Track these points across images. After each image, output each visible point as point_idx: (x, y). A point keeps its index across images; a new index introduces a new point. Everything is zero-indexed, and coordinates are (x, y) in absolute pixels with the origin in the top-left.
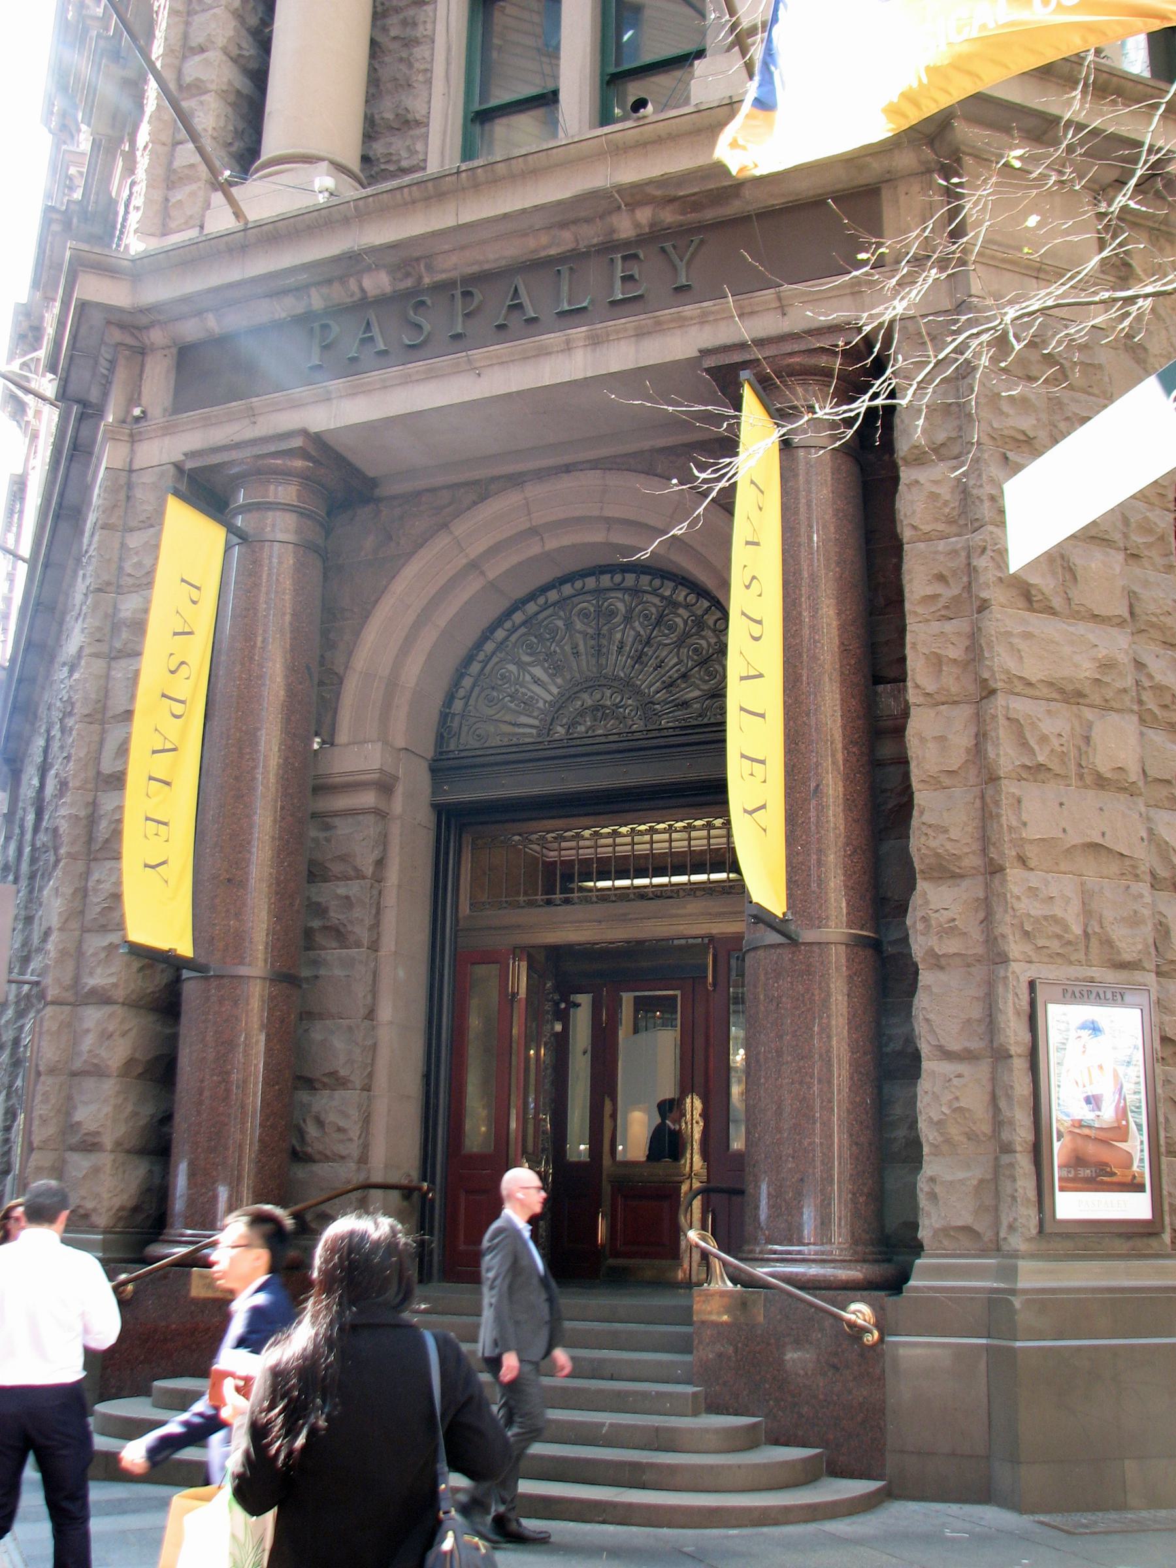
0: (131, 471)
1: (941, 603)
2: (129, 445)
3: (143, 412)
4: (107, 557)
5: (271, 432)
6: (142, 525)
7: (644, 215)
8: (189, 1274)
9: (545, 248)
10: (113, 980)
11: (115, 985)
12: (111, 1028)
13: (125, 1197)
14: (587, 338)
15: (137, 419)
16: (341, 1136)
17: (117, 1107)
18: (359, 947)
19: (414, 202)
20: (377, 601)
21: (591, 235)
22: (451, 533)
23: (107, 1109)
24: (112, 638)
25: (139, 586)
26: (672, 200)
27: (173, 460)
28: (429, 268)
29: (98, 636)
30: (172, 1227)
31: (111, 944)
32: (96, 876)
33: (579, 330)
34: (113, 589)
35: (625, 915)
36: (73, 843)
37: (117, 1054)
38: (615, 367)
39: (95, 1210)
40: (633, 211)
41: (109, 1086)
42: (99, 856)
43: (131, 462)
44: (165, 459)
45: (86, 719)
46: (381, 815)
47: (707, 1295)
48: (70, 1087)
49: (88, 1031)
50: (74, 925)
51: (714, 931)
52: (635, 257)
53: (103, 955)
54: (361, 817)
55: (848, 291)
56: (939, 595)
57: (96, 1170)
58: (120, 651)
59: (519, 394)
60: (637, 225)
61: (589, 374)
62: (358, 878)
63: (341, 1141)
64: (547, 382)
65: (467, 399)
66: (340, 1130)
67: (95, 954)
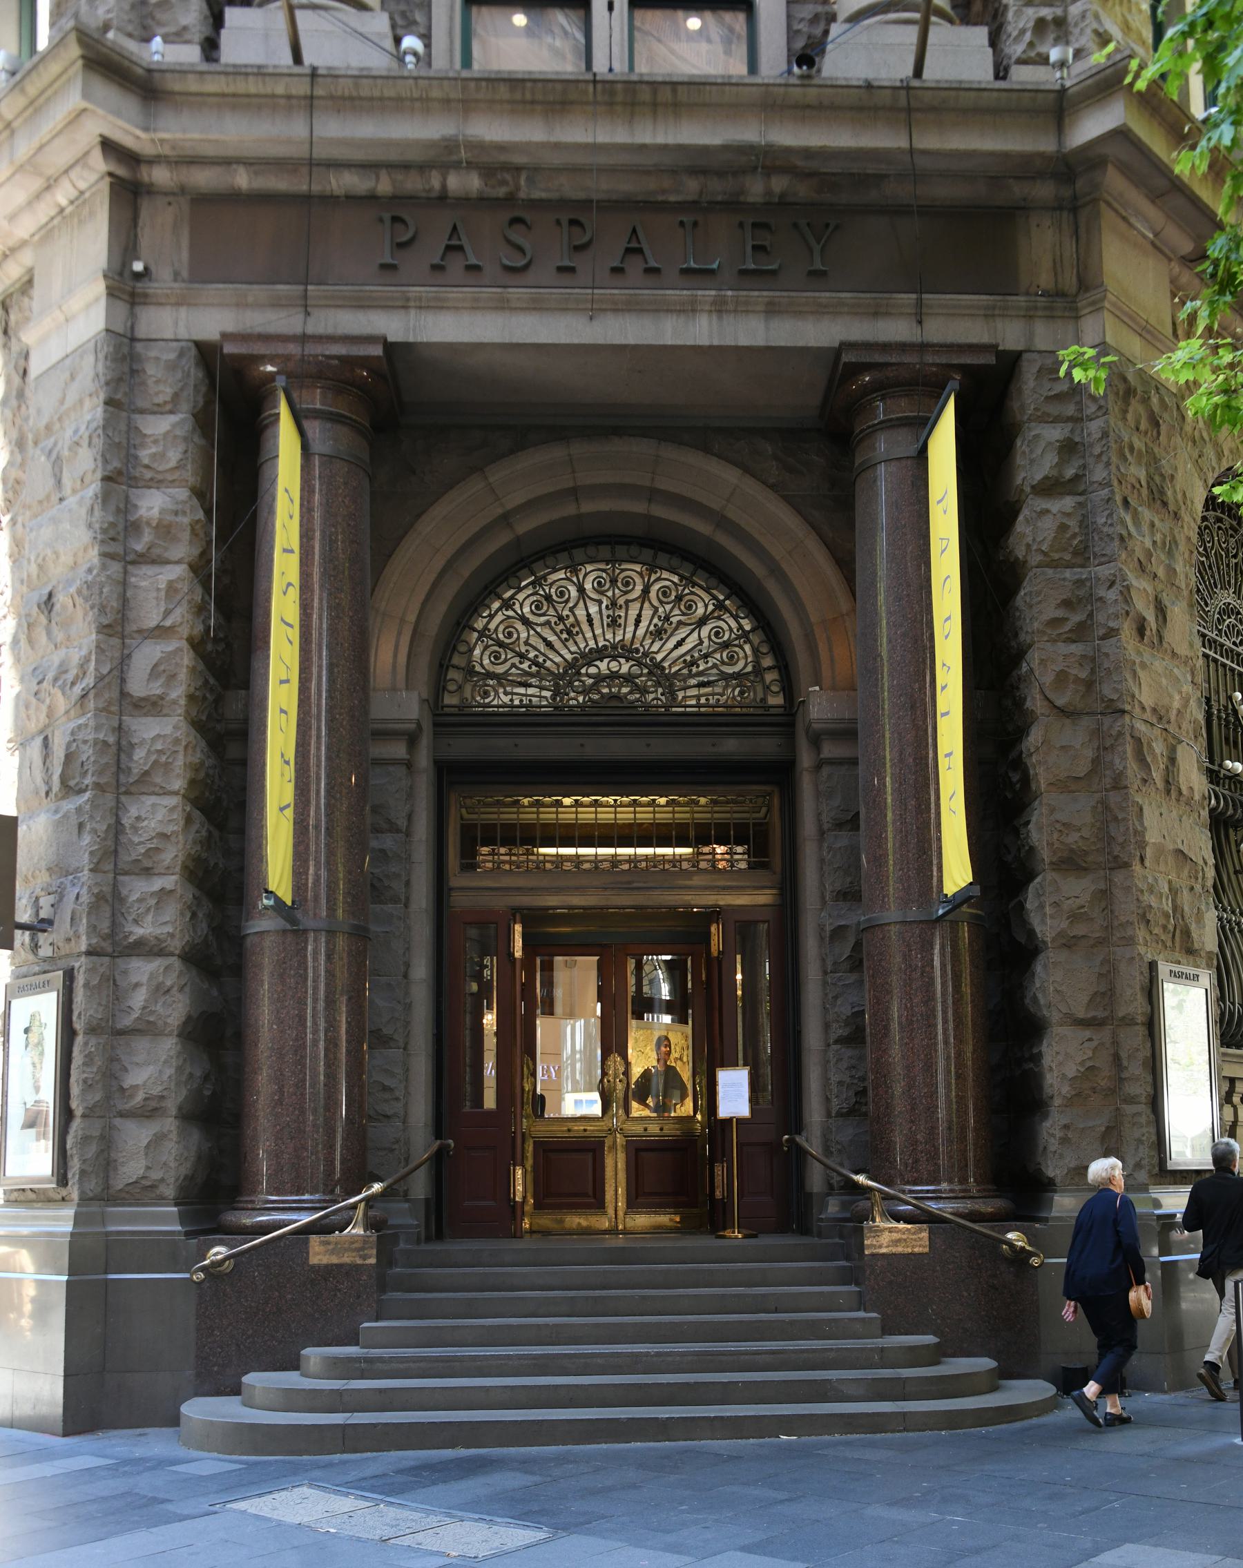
0: (133, 339)
1: (1068, 626)
2: (128, 306)
3: (146, 268)
4: (117, 440)
5: (330, 331)
6: (156, 409)
7: (779, 184)
8: (307, 1242)
9: (664, 192)
10: (169, 929)
11: (172, 935)
12: (169, 983)
13: (189, 1165)
14: (714, 303)
15: (138, 276)
16: (387, 1096)
17: (179, 1069)
18: (396, 903)
19: (533, 102)
20: (401, 538)
21: (718, 188)
22: (486, 478)
23: (170, 1071)
24: (125, 537)
25: (160, 481)
26: (811, 175)
27: (195, 337)
28: (530, 180)
29: (112, 533)
30: (254, 1192)
31: (162, 889)
32: (134, 811)
33: (707, 293)
34: (124, 479)
35: (629, 883)
36: (100, 773)
37: (175, 1011)
38: (744, 341)
39: (162, 1180)
40: (768, 175)
41: (169, 1046)
42: (133, 789)
43: (132, 328)
44: (183, 333)
45: (105, 631)
46: (409, 765)
47: (876, 1231)
48: (113, 1048)
49: (137, 985)
50: (109, 866)
51: (721, 903)
52: (765, 226)
53: (153, 902)
54: (391, 768)
55: (982, 312)
56: (1067, 619)
57: (158, 1139)
58: (142, 555)
59: (636, 347)
60: (769, 192)
61: (716, 342)
62: (390, 831)
63: (386, 1101)
64: (669, 341)
65: (576, 341)
66: (386, 1089)
67: (140, 900)
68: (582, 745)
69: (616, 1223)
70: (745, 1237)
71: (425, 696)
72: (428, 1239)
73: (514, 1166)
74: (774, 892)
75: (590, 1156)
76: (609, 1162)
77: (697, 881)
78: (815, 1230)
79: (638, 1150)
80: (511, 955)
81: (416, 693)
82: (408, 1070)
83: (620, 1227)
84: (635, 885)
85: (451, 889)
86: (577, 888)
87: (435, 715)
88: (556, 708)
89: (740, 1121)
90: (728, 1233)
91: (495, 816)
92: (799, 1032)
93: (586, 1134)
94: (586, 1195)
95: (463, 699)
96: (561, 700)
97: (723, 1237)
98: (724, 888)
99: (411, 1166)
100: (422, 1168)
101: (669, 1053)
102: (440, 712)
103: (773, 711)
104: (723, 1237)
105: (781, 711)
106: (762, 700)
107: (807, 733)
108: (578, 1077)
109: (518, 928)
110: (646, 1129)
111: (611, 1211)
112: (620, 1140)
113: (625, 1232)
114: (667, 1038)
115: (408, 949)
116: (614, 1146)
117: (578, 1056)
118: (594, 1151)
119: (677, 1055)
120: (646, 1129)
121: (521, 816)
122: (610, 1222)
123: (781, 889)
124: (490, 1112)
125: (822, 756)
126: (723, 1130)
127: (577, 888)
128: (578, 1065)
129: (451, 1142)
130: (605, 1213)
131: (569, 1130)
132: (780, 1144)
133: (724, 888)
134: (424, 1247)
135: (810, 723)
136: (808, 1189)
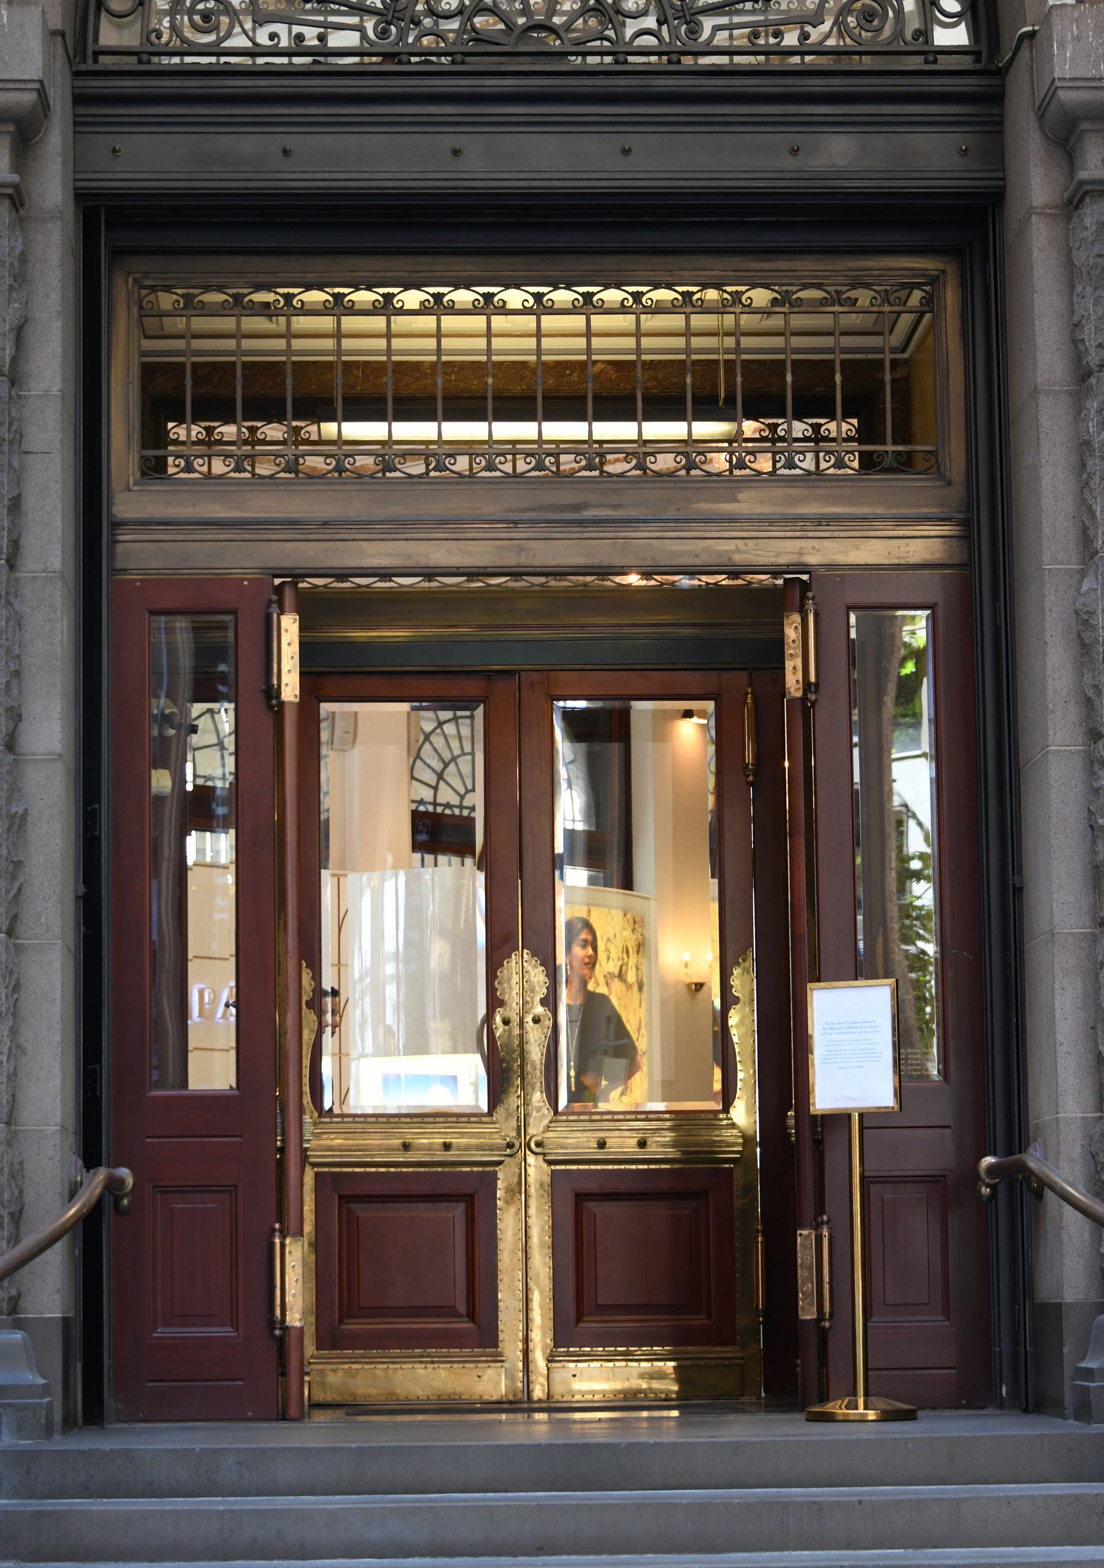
35: (577, 507)
51: (812, 560)
68: (456, 152)
69: (528, 1382)
70: (887, 1416)
71: (56, 22)
72: (69, 1424)
73: (283, 1237)
74: (946, 530)
75: (459, 1211)
76: (507, 1224)
77: (747, 503)
78: (1068, 1399)
79: (581, 1198)
80: (271, 693)
81: (35, 13)
82: (17, 988)
83: (538, 1393)
84: (589, 514)
85: (116, 525)
86: (442, 522)
87: (77, 74)
88: (388, 56)
89: (870, 1119)
90: (837, 1408)
91: (230, 344)
92: (1019, 891)
93: (451, 1156)
94: (450, 1312)
95: (150, 33)
96: (402, 35)
97: (829, 1418)
98: (821, 521)
99: (28, 1242)
100: (59, 1247)
101: (592, 963)
102: (90, 66)
103: (945, 63)
104: (829, 1418)
105: (965, 63)
106: (917, 34)
107: (1041, 118)
108: (390, 1019)
109: (289, 628)
110: (602, 1145)
111: (511, 1347)
112: (536, 1169)
113: (551, 1406)
114: (587, 925)
115: (17, 674)
116: (519, 1187)
117: (390, 969)
118: (469, 1199)
119: (613, 967)
120: (602, 1145)
121: (297, 344)
122: (511, 1377)
123: (965, 523)
124: (211, 1101)
125: (1083, 175)
126: (819, 1144)
127: (442, 522)
128: (391, 991)
129: (124, 1172)
130: (497, 1358)
131: (406, 1147)
132: (974, 1177)
133: (821, 521)
134: (60, 1443)
135: (1052, 90)
136: (1045, 1292)
